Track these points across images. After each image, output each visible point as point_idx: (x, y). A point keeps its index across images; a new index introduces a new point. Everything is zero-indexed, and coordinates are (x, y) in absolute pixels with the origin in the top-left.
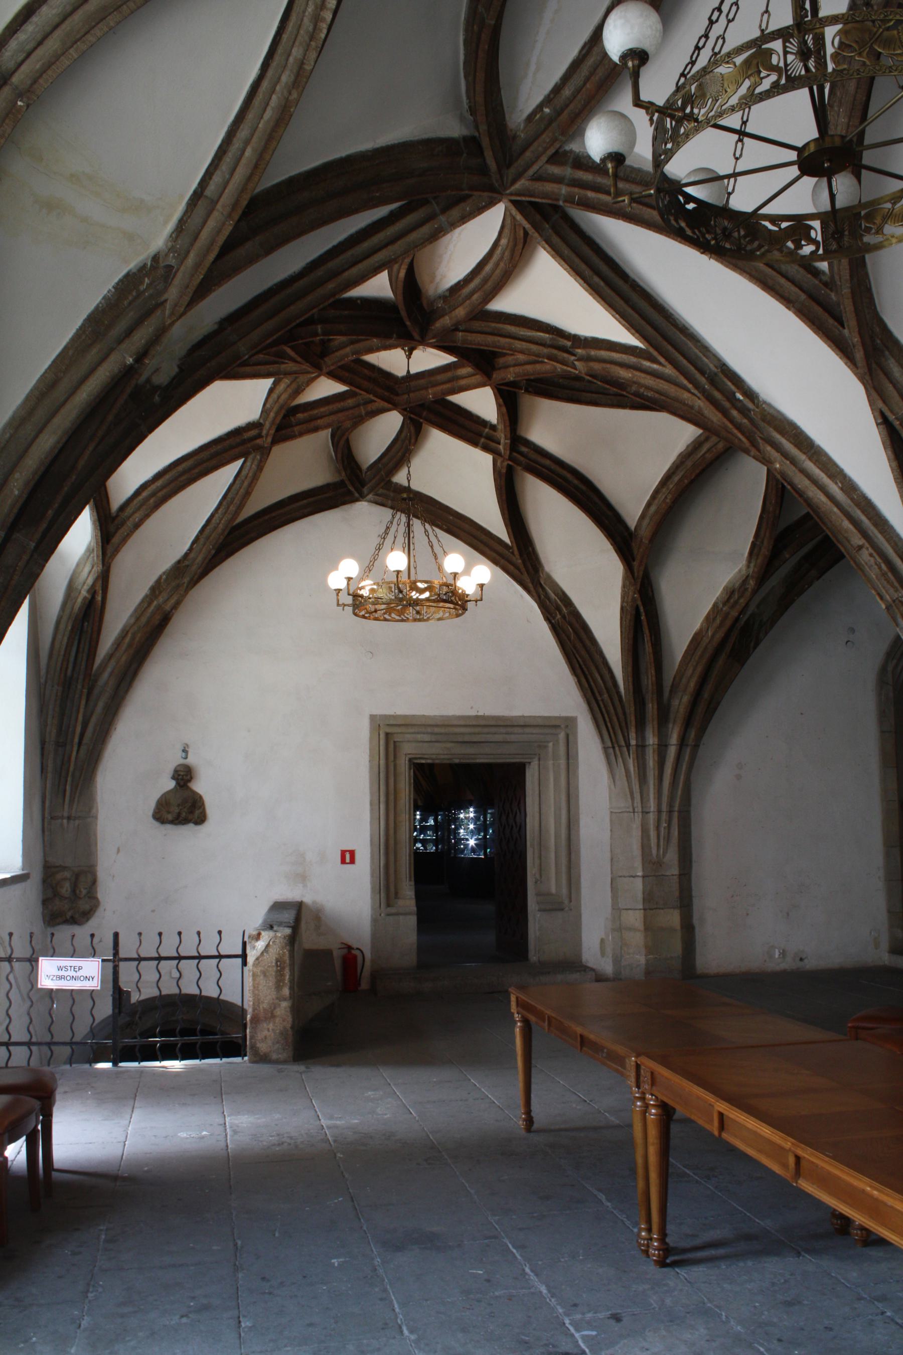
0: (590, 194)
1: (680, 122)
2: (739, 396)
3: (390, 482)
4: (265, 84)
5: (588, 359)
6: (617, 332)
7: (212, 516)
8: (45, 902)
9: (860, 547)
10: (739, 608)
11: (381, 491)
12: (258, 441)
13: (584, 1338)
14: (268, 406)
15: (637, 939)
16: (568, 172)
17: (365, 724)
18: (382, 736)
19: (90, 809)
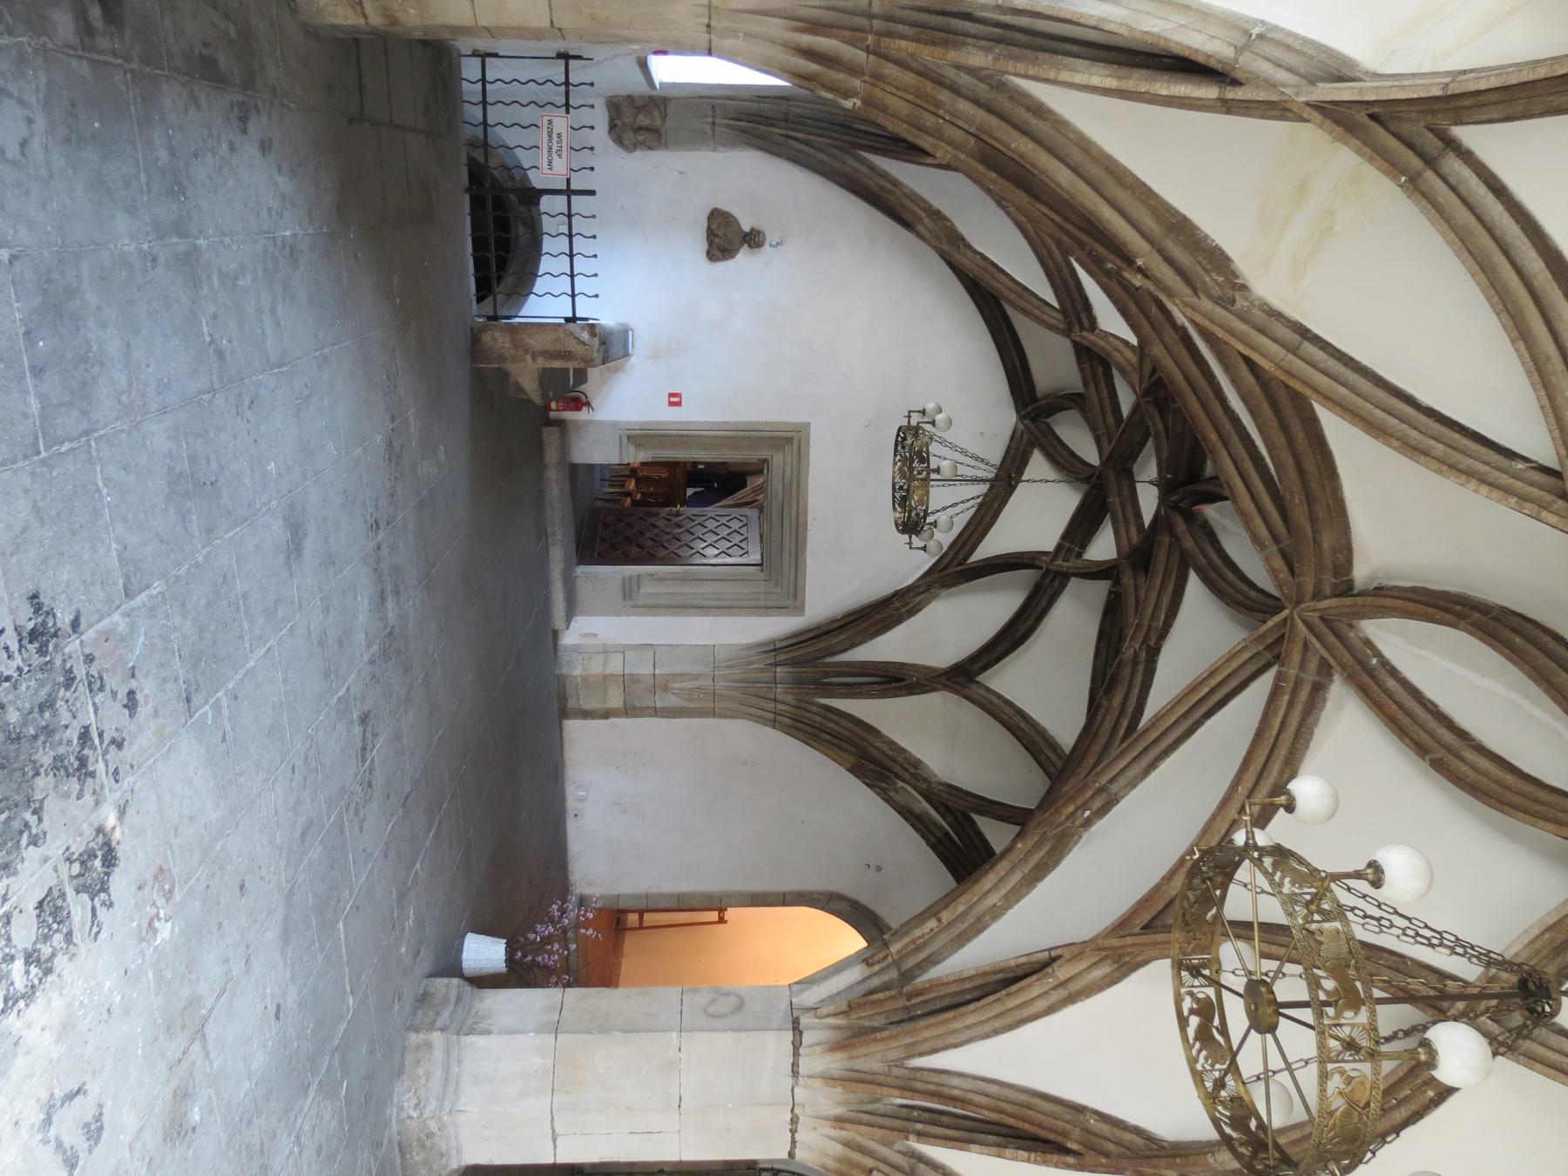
0: (1286, 698)
1: (1307, 904)
2: (1087, 813)
4: (1410, 411)
5: (1135, 663)
6: (1155, 703)
8: (630, 98)
9: (939, 920)
10: (901, 772)
13: (206, 713)
15: (596, 667)
16: (1310, 677)
19: (723, 145)
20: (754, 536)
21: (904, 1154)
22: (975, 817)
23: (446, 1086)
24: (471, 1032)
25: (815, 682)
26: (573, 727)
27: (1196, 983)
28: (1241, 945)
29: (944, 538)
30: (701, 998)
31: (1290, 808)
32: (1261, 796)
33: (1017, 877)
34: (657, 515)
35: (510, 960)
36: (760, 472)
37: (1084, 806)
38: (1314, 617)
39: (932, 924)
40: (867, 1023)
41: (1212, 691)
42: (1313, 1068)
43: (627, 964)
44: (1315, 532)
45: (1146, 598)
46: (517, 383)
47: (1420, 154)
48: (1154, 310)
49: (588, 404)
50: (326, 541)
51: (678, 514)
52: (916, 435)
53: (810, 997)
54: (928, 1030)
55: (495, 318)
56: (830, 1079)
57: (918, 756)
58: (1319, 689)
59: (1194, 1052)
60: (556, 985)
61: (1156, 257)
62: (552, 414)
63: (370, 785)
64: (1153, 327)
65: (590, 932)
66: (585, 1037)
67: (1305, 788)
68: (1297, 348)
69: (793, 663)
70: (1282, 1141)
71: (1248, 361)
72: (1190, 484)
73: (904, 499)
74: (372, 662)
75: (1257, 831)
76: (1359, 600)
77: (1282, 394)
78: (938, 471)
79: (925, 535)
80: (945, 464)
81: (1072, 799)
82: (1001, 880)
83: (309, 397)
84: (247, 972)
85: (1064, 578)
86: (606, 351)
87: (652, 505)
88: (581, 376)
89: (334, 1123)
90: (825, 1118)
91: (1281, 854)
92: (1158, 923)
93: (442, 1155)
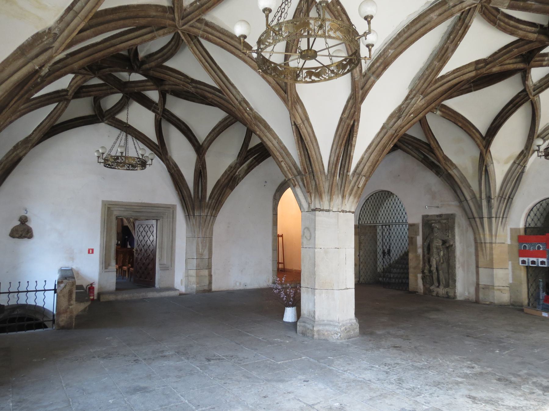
0: (210, 36)
3: (114, 117)
5: (197, 88)
6: (210, 81)
7: (43, 122)
9: (282, 161)
10: (233, 172)
11: (110, 120)
12: (67, 97)
14: (72, 84)
15: (193, 280)
16: (203, 26)
17: (100, 204)
18: (106, 208)
20: (147, 222)
21: (353, 177)
22: (249, 148)
23: (331, 325)
24: (314, 317)
25: (200, 201)
26: (214, 287)
27: (301, 76)
28: (290, 59)
29: (148, 152)
30: (305, 241)
31: (245, 37)
32: (241, 47)
33: (268, 134)
34: (137, 258)
35: (292, 306)
36: (122, 220)
37: (245, 110)
38: (182, 22)
39: (283, 164)
40: (314, 187)
41: (207, 62)
42: (329, 40)
43: (295, 268)
44: (149, 17)
45: (173, 82)
46: (82, 311)
48: (59, 65)
49: (92, 284)
50: (141, 378)
51: (137, 250)
52: (108, 160)
53: (305, 205)
54: (316, 167)
55: (54, 321)
56: (331, 200)
57: (228, 166)
58: (207, 24)
60: (300, 290)
61: (35, 61)
62: (95, 298)
63: (232, 356)
64: (65, 67)
65: (283, 279)
66: (316, 279)
67: (238, 30)
68: (76, 12)
69: (193, 209)
70: (350, 53)
71: (80, 32)
72: (131, 61)
73: (133, 166)
74: (188, 359)
75: (253, 49)
76: (176, 5)
77: (95, 21)
78: (122, 153)
79: (147, 159)
80: (119, 150)
81: (243, 114)
82: (269, 140)
83: (83, 390)
84: (293, 392)
85: (165, 111)
86: (69, 277)
87: (133, 260)
88: (80, 287)
89: (341, 360)
90: (342, 202)
91: (260, 42)
92: (284, 88)
93: (352, 325)
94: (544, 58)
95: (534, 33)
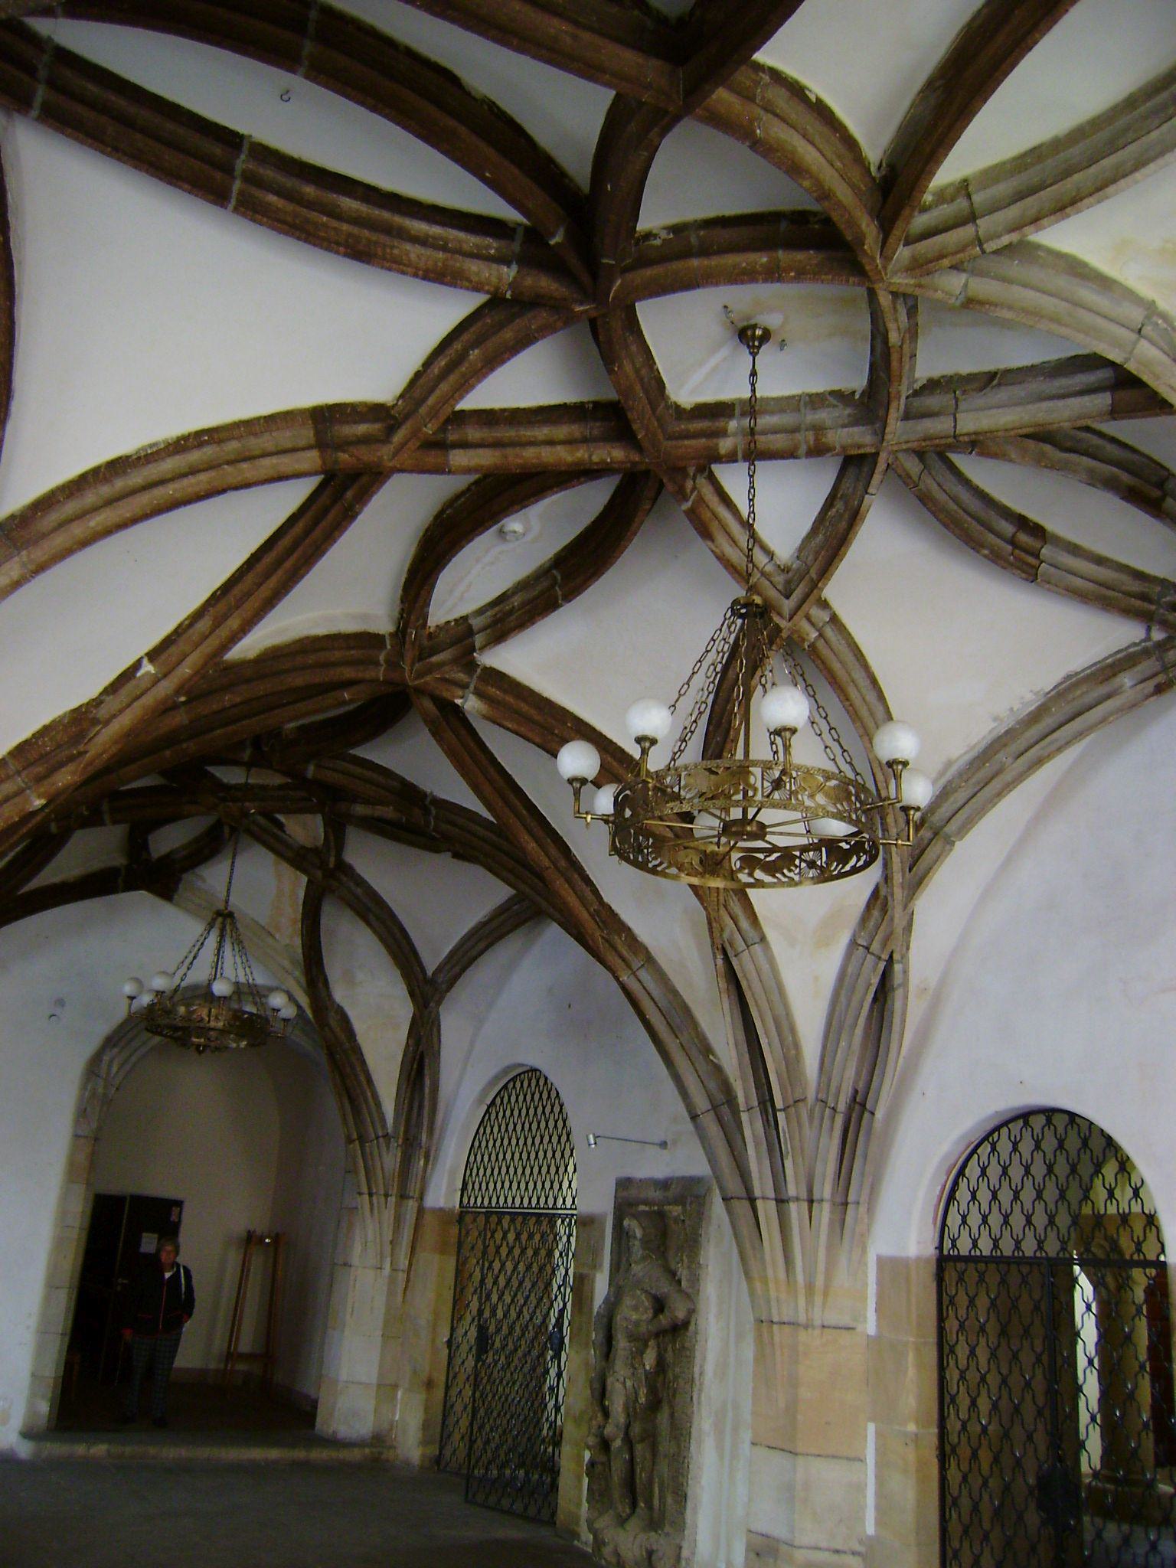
47: (369, 1188)
59: (784, 880)
94: (720, 424)
95: (502, 260)
